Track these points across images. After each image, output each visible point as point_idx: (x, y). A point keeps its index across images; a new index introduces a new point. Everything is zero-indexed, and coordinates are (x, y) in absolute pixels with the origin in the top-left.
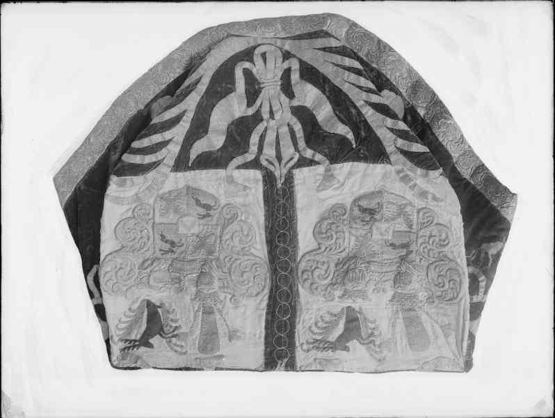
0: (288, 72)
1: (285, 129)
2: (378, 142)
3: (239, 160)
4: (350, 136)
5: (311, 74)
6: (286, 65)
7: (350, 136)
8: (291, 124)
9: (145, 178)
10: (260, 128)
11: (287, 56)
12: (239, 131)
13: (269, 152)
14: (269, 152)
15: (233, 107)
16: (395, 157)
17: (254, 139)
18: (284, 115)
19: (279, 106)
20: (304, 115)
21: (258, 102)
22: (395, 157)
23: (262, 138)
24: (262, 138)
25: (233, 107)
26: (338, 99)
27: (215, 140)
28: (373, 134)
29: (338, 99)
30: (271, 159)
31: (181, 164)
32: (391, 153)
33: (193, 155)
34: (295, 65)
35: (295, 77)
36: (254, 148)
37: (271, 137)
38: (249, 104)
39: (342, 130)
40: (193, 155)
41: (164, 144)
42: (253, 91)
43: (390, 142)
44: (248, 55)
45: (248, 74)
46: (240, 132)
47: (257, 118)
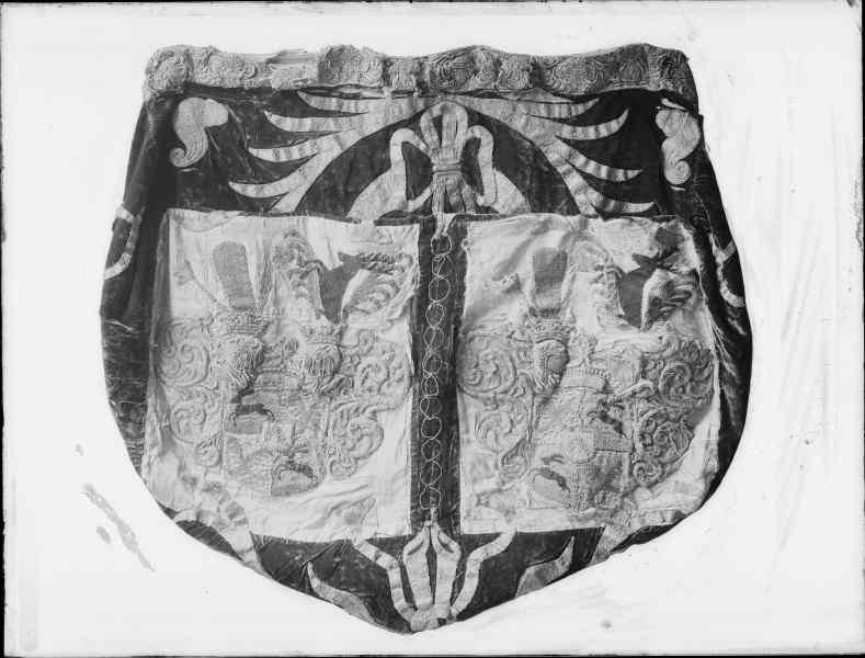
0: (472, 146)
35: (485, 154)
36: (473, 568)
37: (444, 589)
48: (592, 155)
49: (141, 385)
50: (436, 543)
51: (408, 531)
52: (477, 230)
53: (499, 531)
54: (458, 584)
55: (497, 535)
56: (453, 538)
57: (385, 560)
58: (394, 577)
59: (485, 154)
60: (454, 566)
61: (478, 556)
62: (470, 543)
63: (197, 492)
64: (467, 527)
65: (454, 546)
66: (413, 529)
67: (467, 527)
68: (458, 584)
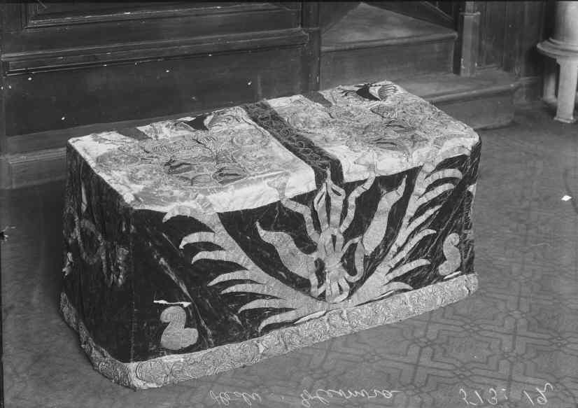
2: (232, 233)
5: (302, 285)
7: (262, 233)
10: (346, 224)
18: (323, 239)
20: (307, 246)
27: (388, 200)
30: (335, 195)
33: (401, 189)
34: (317, 291)
35: (314, 280)
36: (352, 202)
37: (335, 218)
39: (267, 236)
40: (401, 189)
41: (430, 188)
43: (220, 236)
44: (354, 288)
45: (353, 272)
47: (349, 234)
48: (122, 131)
49: (260, 93)
50: (330, 192)
51: (313, 186)
52: (353, 167)
53: (367, 178)
54: (344, 214)
55: (365, 181)
56: (341, 186)
57: (300, 209)
58: (308, 217)
59: (314, 280)
60: (341, 202)
61: (355, 194)
62: (349, 187)
63: (270, 115)
64: (348, 178)
65: (342, 191)
66: (317, 186)
67: (348, 178)
68: (344, 214)
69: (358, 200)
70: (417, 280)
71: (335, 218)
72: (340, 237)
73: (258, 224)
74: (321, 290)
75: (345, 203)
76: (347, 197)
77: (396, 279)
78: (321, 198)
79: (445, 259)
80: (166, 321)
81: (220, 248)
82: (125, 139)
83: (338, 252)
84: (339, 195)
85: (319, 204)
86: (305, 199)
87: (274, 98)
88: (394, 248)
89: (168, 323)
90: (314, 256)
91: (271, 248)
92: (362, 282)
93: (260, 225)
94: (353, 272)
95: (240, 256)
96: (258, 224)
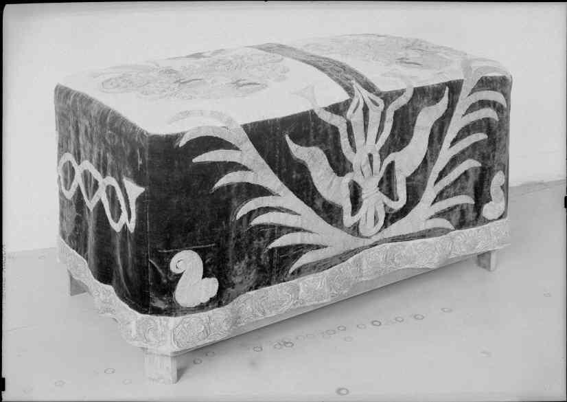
1: (359, 141)
2: (261, 150)
3: (402, 101)
4: (293, 147)
5: (330, 213)
6: (356, 219)
7: (293, 147)
8: (299, 217)
9: (9, 258)
10: (381, 142)
11: (355, 230)
12: (370, 44)
13: (374, 116)
14: (374, 116)
15: (407, 160)
16: (237, 136)
17: (388, 126)
18: (357, 159)
19: (364, 170)
20: (339, 165)
21: (384, 169)
22: (237, 136)
23: (381, 129)
24: (381, 129)
25: (407, 160)
26: (303, 187)
27: (426, 119)
28: (266, 157)
29: (303, 187)
30: (374, 106)
31: (454, 88)
32: (245, 142)
33: (445, 100)
34: (348, 220)
35: (347, 205)
36: (390, 115)
37: (373, 131)
38: (391, 166)
39: (299, 152)
40: (445, 100)
41: (472, 108)
42: (387, 185)
43: (248, 154)
44: (392, 217)
45: (391, 194)
46: (400, 137)
47: (385, 151)
69: (396, 113)
70: (466, 219)
71: (373, 131)
72: (376, 156)
73: (287, 138)
74: (356, 219)
75: (383, 115)
76: (385, 109)
77: (440, 215)
78: (357, 107)
79: (491, 200)
80: (178, 272)
81: (245, 168)
82: (131, 241)
83: (376, 174)
84: (377, 105)
85: (356, 117)
86: (336, 109)
87: (176, 285)
88: (433, 176)
89: (180, 275)
90: (347, 179)
91: (302, 167)
92: (404, 212)
93: (291, 138)
94: (391, 194)
95: (268, 179)
96: (287, 138)
